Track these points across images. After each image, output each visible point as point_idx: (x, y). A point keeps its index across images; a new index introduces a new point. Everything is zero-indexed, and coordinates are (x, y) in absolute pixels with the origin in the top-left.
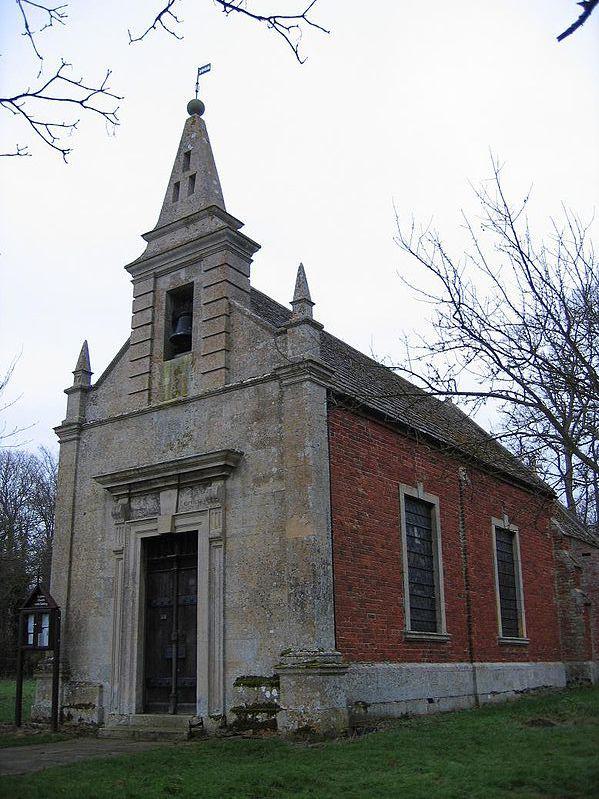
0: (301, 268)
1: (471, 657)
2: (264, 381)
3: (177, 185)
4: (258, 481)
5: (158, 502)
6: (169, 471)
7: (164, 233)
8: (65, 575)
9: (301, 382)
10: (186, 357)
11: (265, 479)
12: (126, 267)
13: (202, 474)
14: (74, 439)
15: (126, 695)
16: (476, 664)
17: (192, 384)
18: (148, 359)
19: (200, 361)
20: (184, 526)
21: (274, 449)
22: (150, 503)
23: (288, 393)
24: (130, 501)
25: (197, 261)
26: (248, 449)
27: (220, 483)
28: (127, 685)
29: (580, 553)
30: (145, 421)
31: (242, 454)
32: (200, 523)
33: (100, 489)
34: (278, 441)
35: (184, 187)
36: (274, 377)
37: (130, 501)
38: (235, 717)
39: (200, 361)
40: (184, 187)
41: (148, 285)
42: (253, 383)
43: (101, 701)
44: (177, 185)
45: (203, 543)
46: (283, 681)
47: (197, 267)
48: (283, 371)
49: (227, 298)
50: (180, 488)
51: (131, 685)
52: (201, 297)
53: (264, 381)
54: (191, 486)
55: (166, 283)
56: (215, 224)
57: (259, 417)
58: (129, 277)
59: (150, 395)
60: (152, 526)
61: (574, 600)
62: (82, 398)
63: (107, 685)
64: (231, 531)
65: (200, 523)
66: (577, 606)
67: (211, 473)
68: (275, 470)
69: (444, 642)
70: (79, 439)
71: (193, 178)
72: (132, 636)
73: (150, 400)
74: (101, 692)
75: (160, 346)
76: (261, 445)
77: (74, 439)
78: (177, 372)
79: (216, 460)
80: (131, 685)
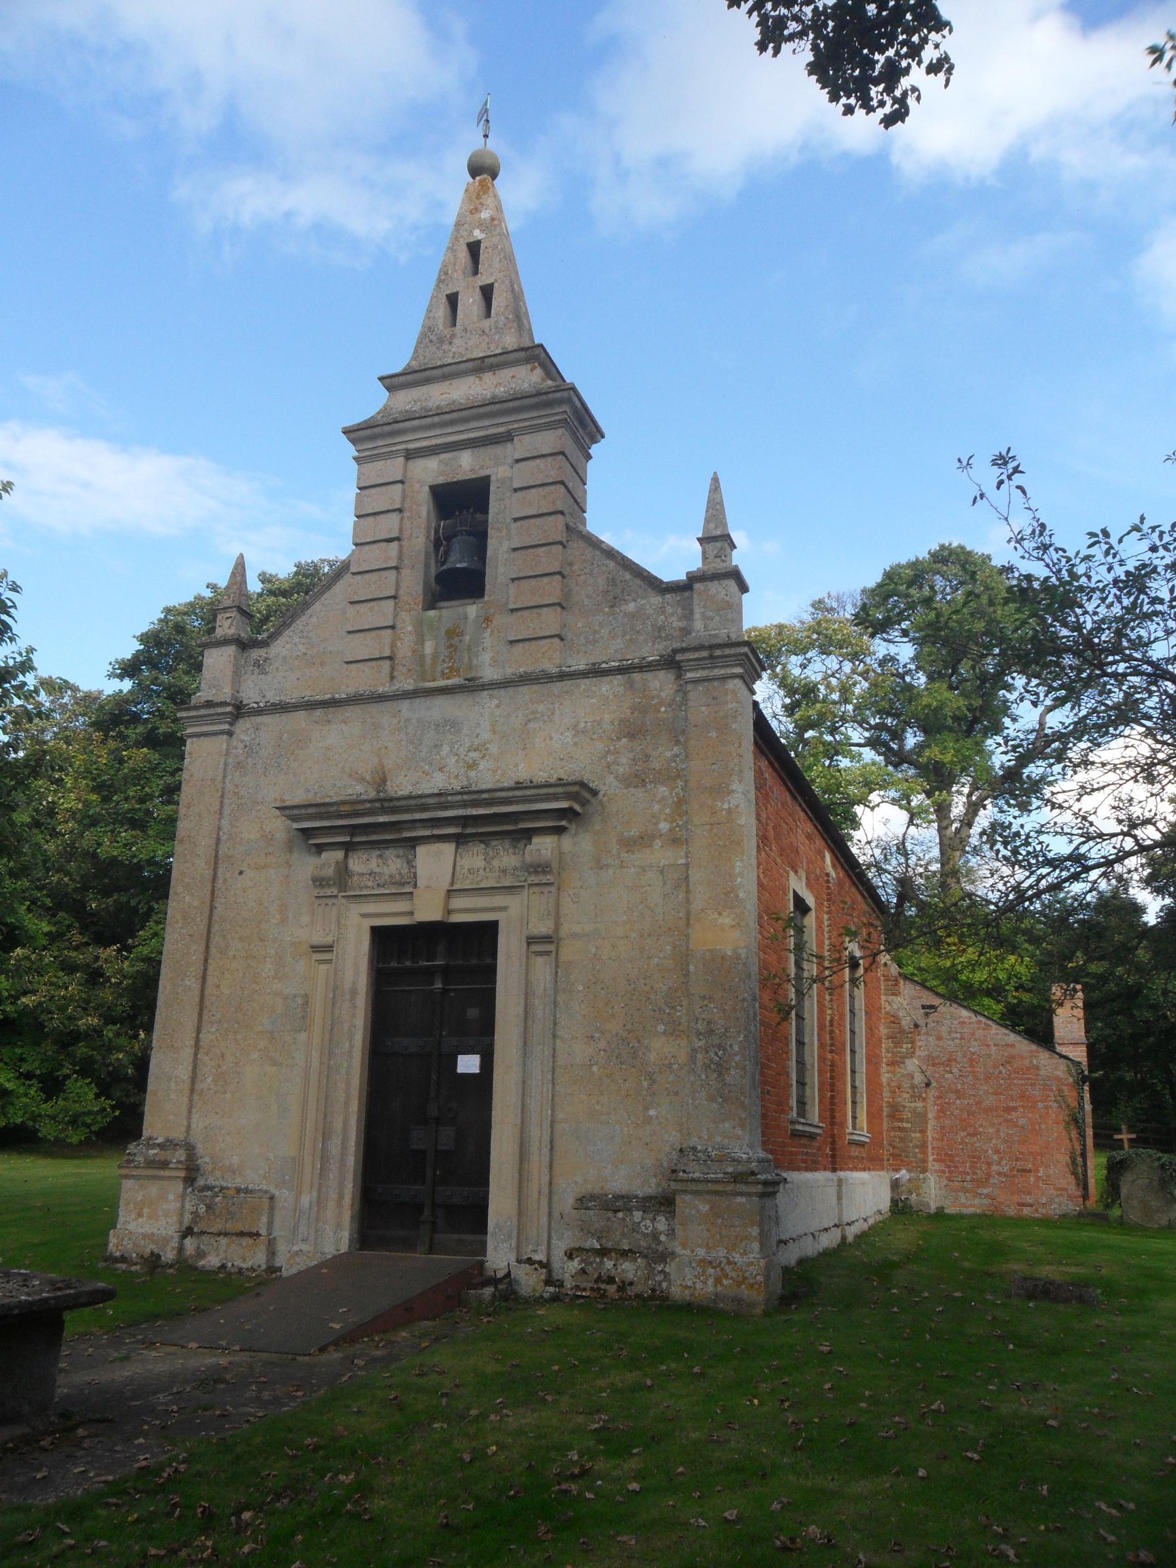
0: (715, 480)
1: (834, 1162)
2: (644, 667)
3: (453, 300)
4: (631, 844)
5: (410, 864)
6: (446, 808)
7: (428, 381)
8: (193, 984)
9: (724, 678)
10: (472, 610)
11: (643, 841)
12: (347, 432)
13: (400, 830)
14: (222, 733)
15: (330, 1212)
16: (842, 1174)
17: (486, 657)
18: (391, 602)
19: (500, 620)
20: (467, 911)
21: (663, 790)
22: (392, 864)
23: (696, 695)
24: (346, 857)
25: (508, 437)
26: (609, 786)
27: (339, 855)
28: (334, 1195)
29: (918, 1004)
30: (382, 714)
31: (595, 793)
32: (504, 909)
33: (280, 827)
34: (671, 776)
35: (470, 303)
36: (670, 662)
37: (346, 857)
38: (575, 1265)
39: (500, 620)
40: (470, 303)
41: (394, 468)
42: (620, 670)
43: (270, 1224)
44: (453, 300)
45: (509, 948)
46: (683, 1203)
47: (498, 450)
48: (691, 656)
49: (562, 513)
50: (460, 840)
51: (341, 1197)
52: (501, 507)
53: (644, 667)
54: (484, 838)
55: (430, 471)
56: (527, 378)
57: (632, 731)
58: (351, 450)
59: (393, 668)
60: (401, 906)
61: (911, 1076)
62: (236, 658)
63: (284, 1196)
64: (565, 930)
65: (504, 909)
66: (913, 1087)
67: (532, 820)
68: (664, 826)
69: (812, 1137)
70: (230, 734)
71: (487, 292)
72: (347, 1104)
73: (392, 677)
74: (272, 1208)
75: (413, 583)
76: (637, 779)
77: (222, 733)
78: (453, 633)
79: (555, 797)
80: (341, 1197)
